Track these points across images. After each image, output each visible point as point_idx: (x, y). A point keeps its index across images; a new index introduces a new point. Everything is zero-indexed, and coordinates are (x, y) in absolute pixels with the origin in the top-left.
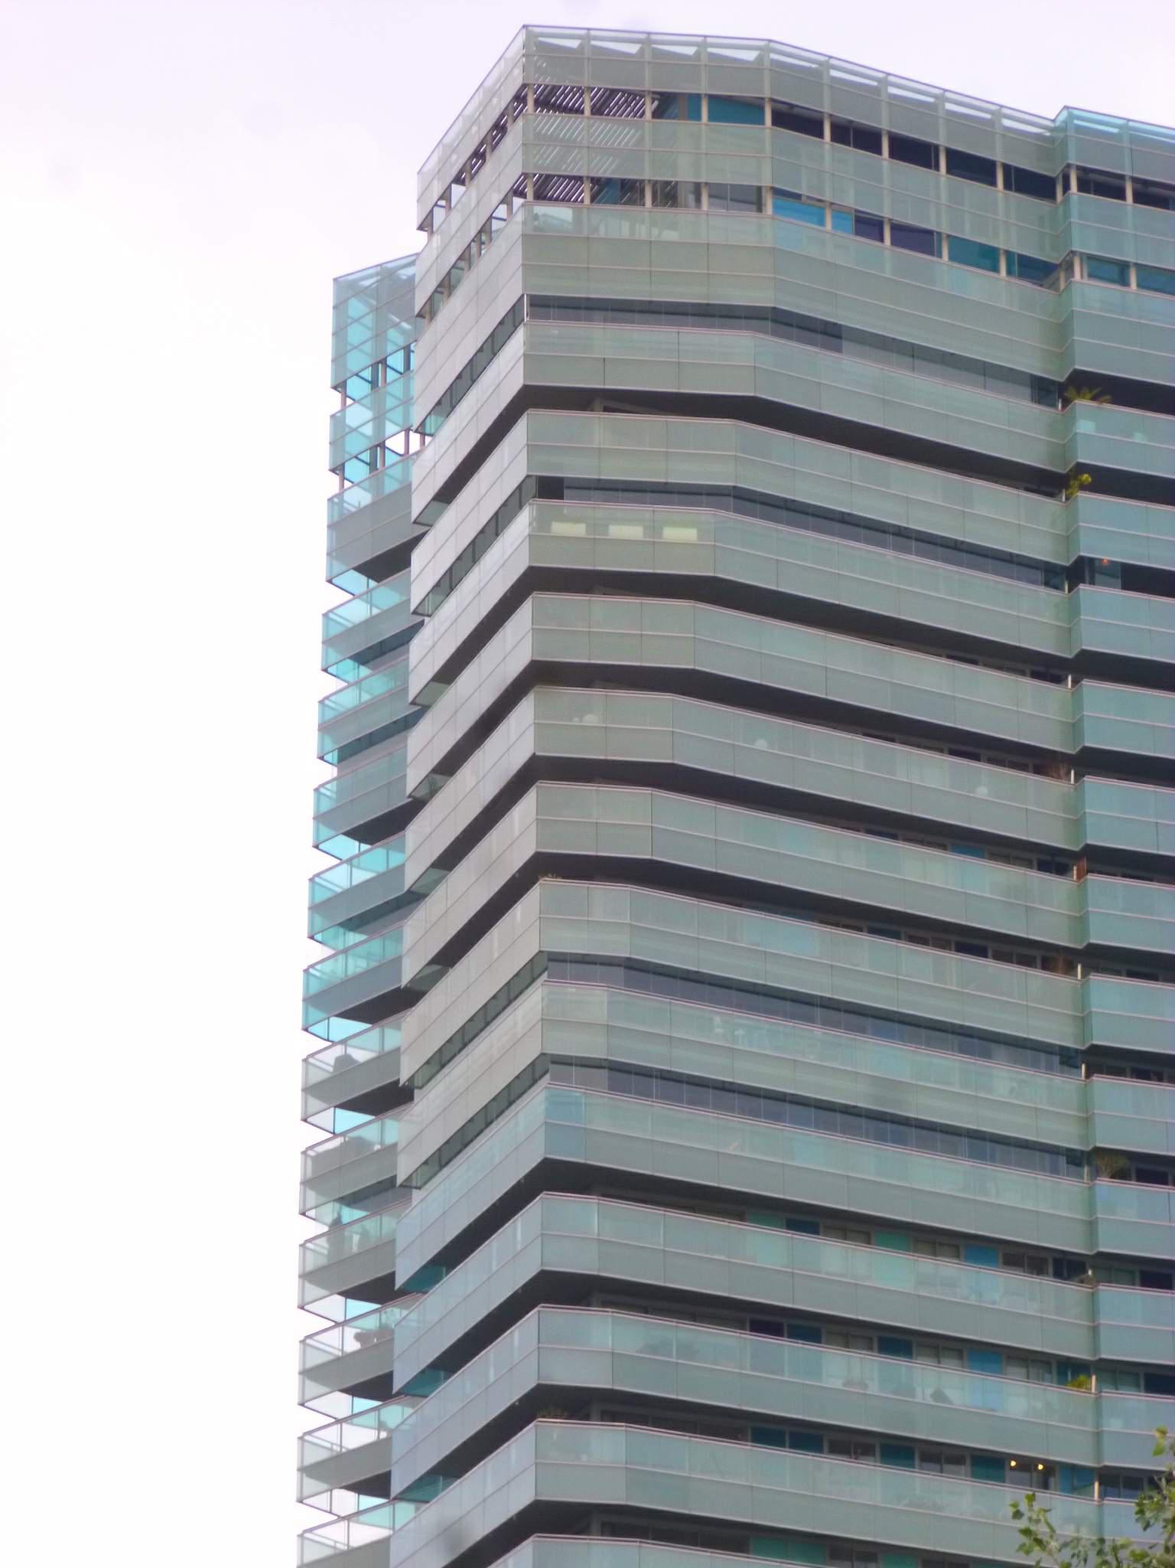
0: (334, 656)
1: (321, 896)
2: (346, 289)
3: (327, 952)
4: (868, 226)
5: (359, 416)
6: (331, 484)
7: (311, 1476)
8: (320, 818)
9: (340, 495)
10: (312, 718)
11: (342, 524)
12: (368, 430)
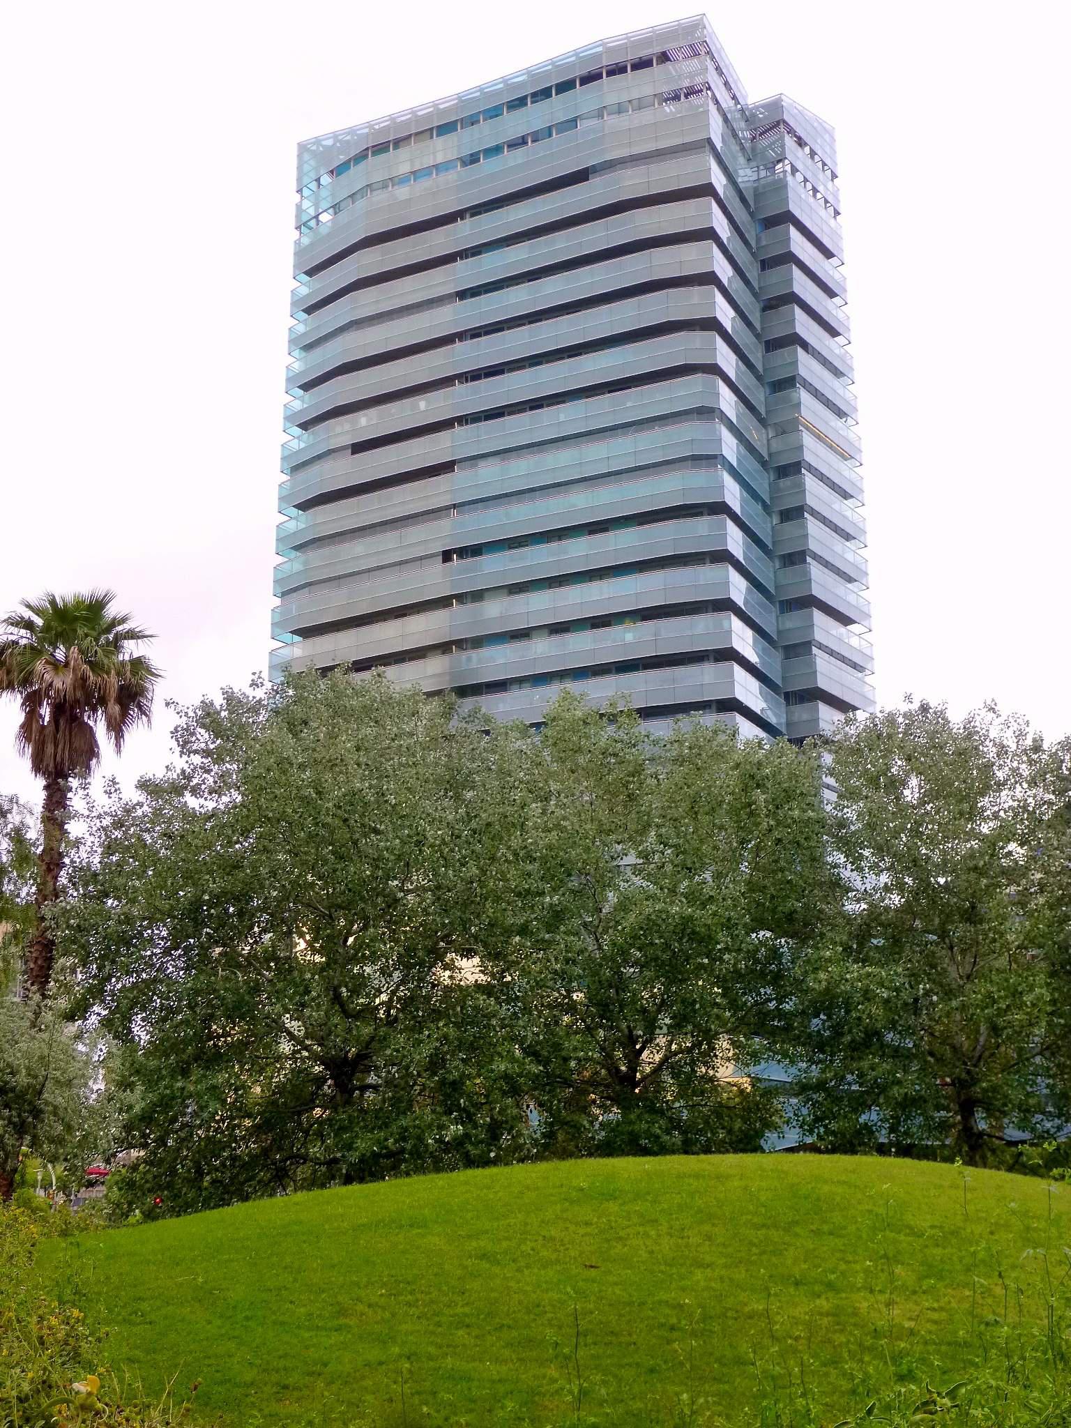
0: (281, 548)
1: (287, 453)
2: (303, 148)
5: (306, 204)
8: (281, 499)
11: (300, 253)
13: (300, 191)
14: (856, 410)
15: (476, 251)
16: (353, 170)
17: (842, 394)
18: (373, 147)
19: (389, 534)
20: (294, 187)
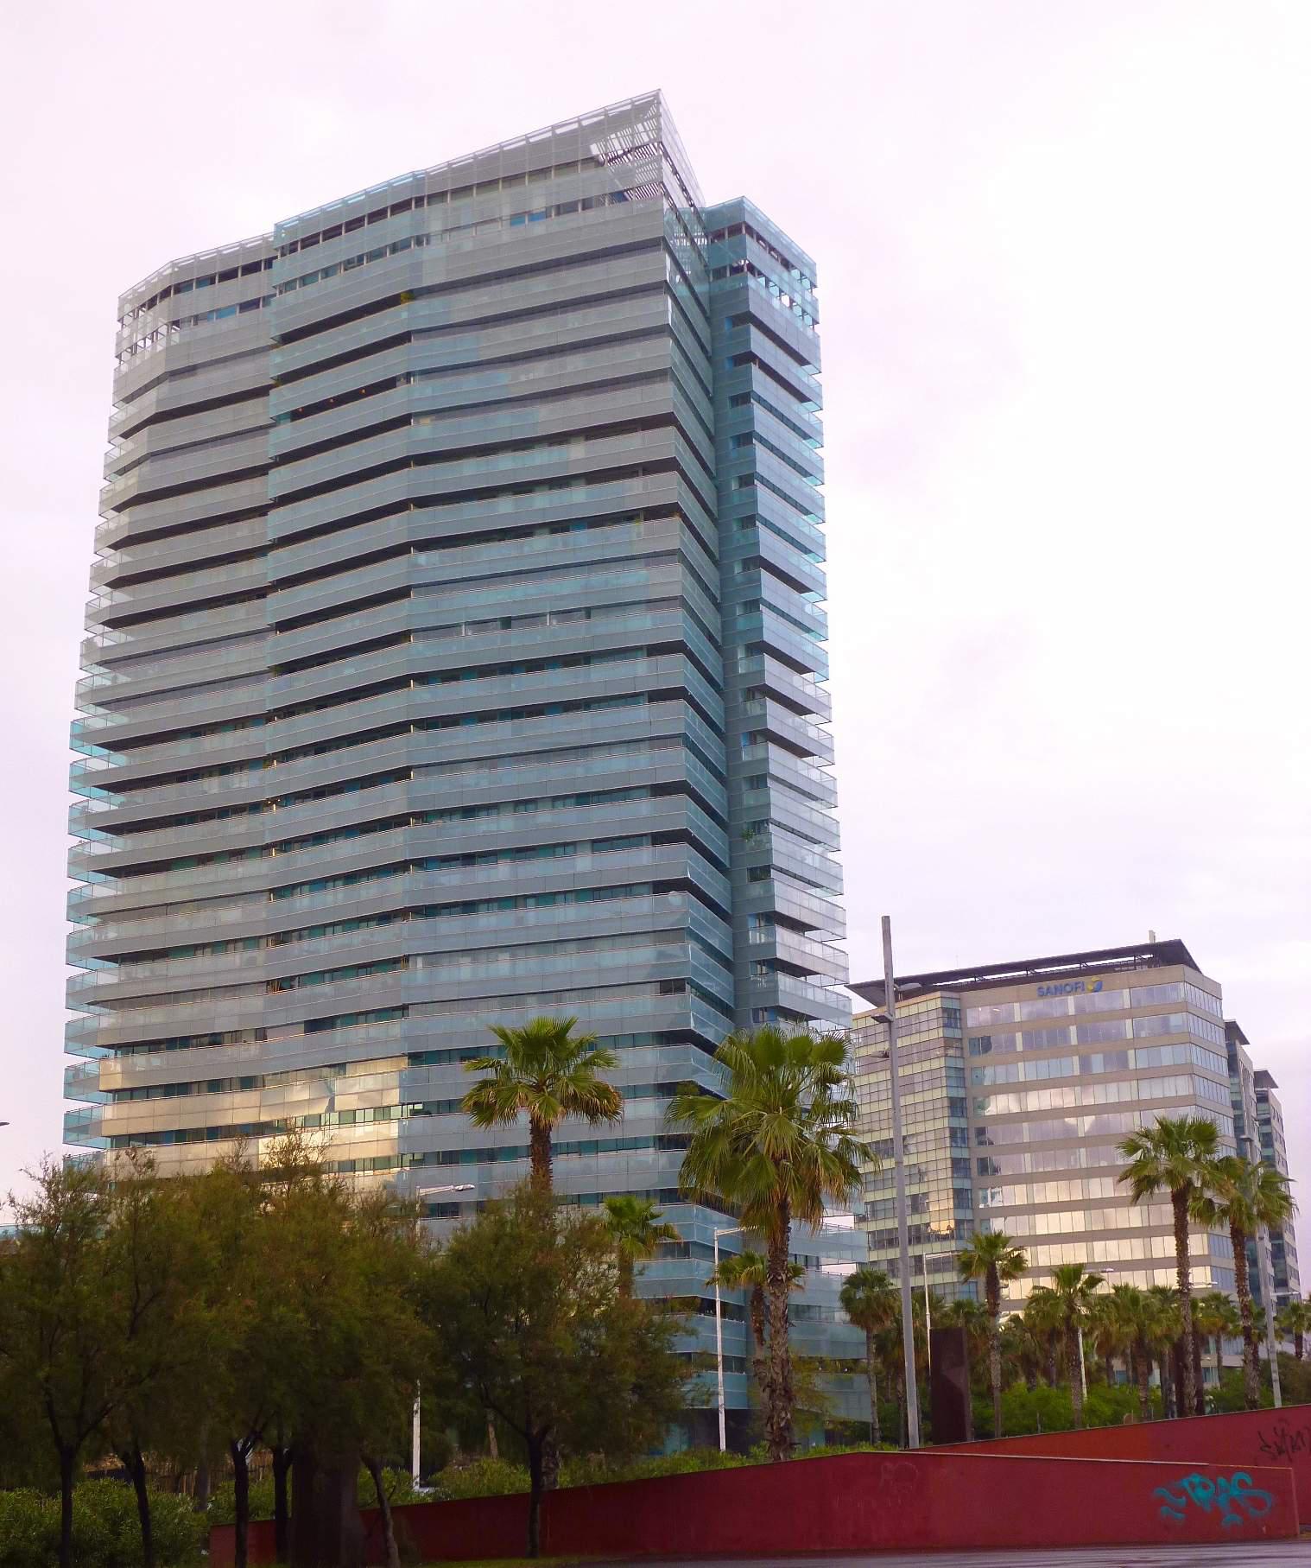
0: (85, 662)
4: (246, 306)
11: (120, 380)
13: (121, 320)
14: (820, 396)
15: (319, 838)
17: (807, 532)
19: (191, 657)
20: (113, 353)
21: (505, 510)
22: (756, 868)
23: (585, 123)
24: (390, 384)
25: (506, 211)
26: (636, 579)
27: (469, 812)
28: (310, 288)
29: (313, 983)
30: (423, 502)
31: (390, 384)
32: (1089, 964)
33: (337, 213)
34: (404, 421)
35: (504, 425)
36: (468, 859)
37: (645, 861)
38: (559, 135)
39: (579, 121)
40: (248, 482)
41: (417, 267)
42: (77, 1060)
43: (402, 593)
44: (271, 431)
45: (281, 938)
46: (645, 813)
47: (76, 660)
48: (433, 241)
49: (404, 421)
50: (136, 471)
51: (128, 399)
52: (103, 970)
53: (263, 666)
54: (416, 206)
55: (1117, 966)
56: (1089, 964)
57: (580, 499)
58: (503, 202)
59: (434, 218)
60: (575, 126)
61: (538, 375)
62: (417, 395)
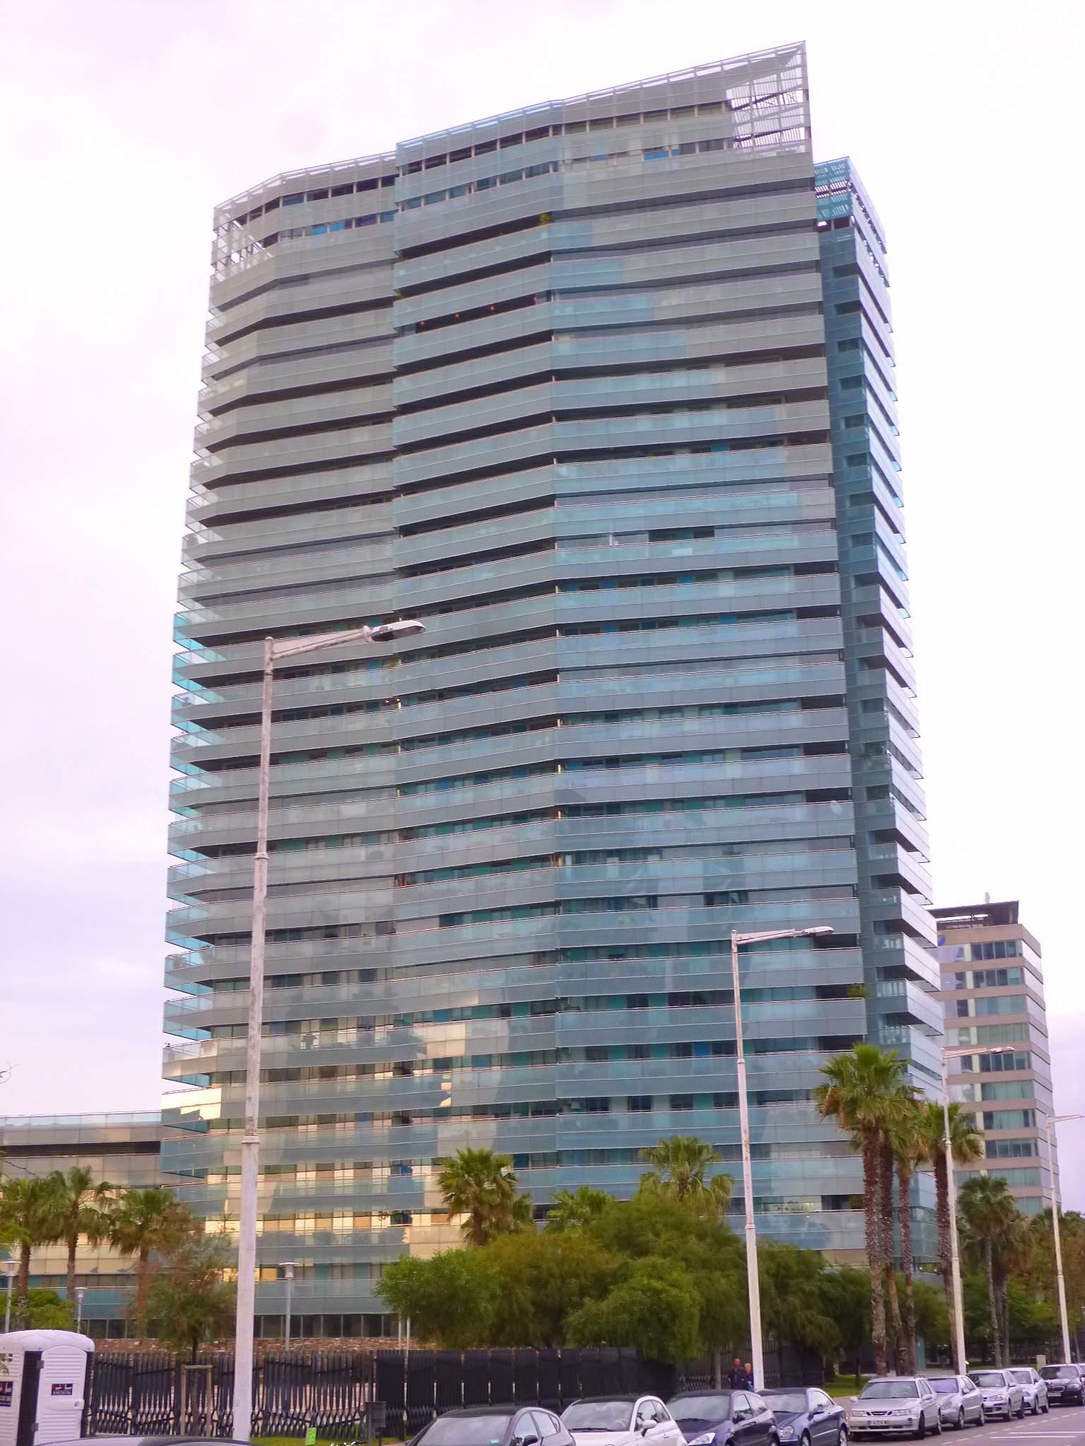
0: (187, 558)
3: (188, 570)
5: (222, 243)
6: (212, 270)
7: (179, 673)
9: (214, 275)
10: (191, 436)
11: (216, 288)
12: (225, 250)
13: (216, 230)
16: (264, 216)
18: (285, 197)
19: (286, 559)
21: (644, 428)
22: (874, 787)
23: (727, 68)
24: (527, 301)
25: (675, 142)
26: (782, 500)
27: (612, 716)
28: (457, 201)
29: (442, 878)
30: (563, 416)
31: (527, 301)
32: (976, 916)
33: (418, 149)
34: (545, 337)
35: (641, 347)
36: (613, 762)
37: (798, 770)
38: (699, 77)
39: (668, 78)
40: (338, 394)
41: (558, 190)
42: (178, 950)
43: (547, 502)
44: (396, 340)
45: (408, 834)
46: (795, 724)
47: (178, 555)
48: (562, 169)
49: (545, 337)
50: (244, 372)
51: (223, 308)
52: (196, 862)
53: (388, 568)
54: (554, 134)
55: (948, 924)
56: (976, 916)
57: (720, 422)
58: (635, 137)
59: (563, 147)
60: (718, 69)
61: (674, 302)
62: (557, 313)
